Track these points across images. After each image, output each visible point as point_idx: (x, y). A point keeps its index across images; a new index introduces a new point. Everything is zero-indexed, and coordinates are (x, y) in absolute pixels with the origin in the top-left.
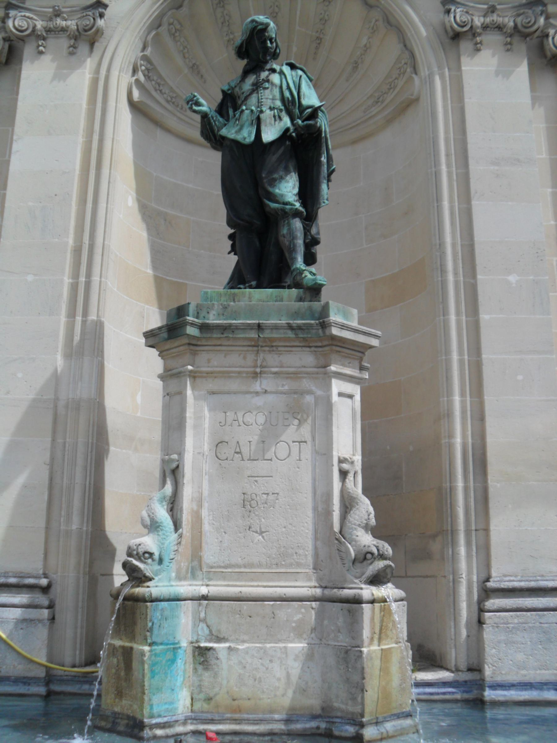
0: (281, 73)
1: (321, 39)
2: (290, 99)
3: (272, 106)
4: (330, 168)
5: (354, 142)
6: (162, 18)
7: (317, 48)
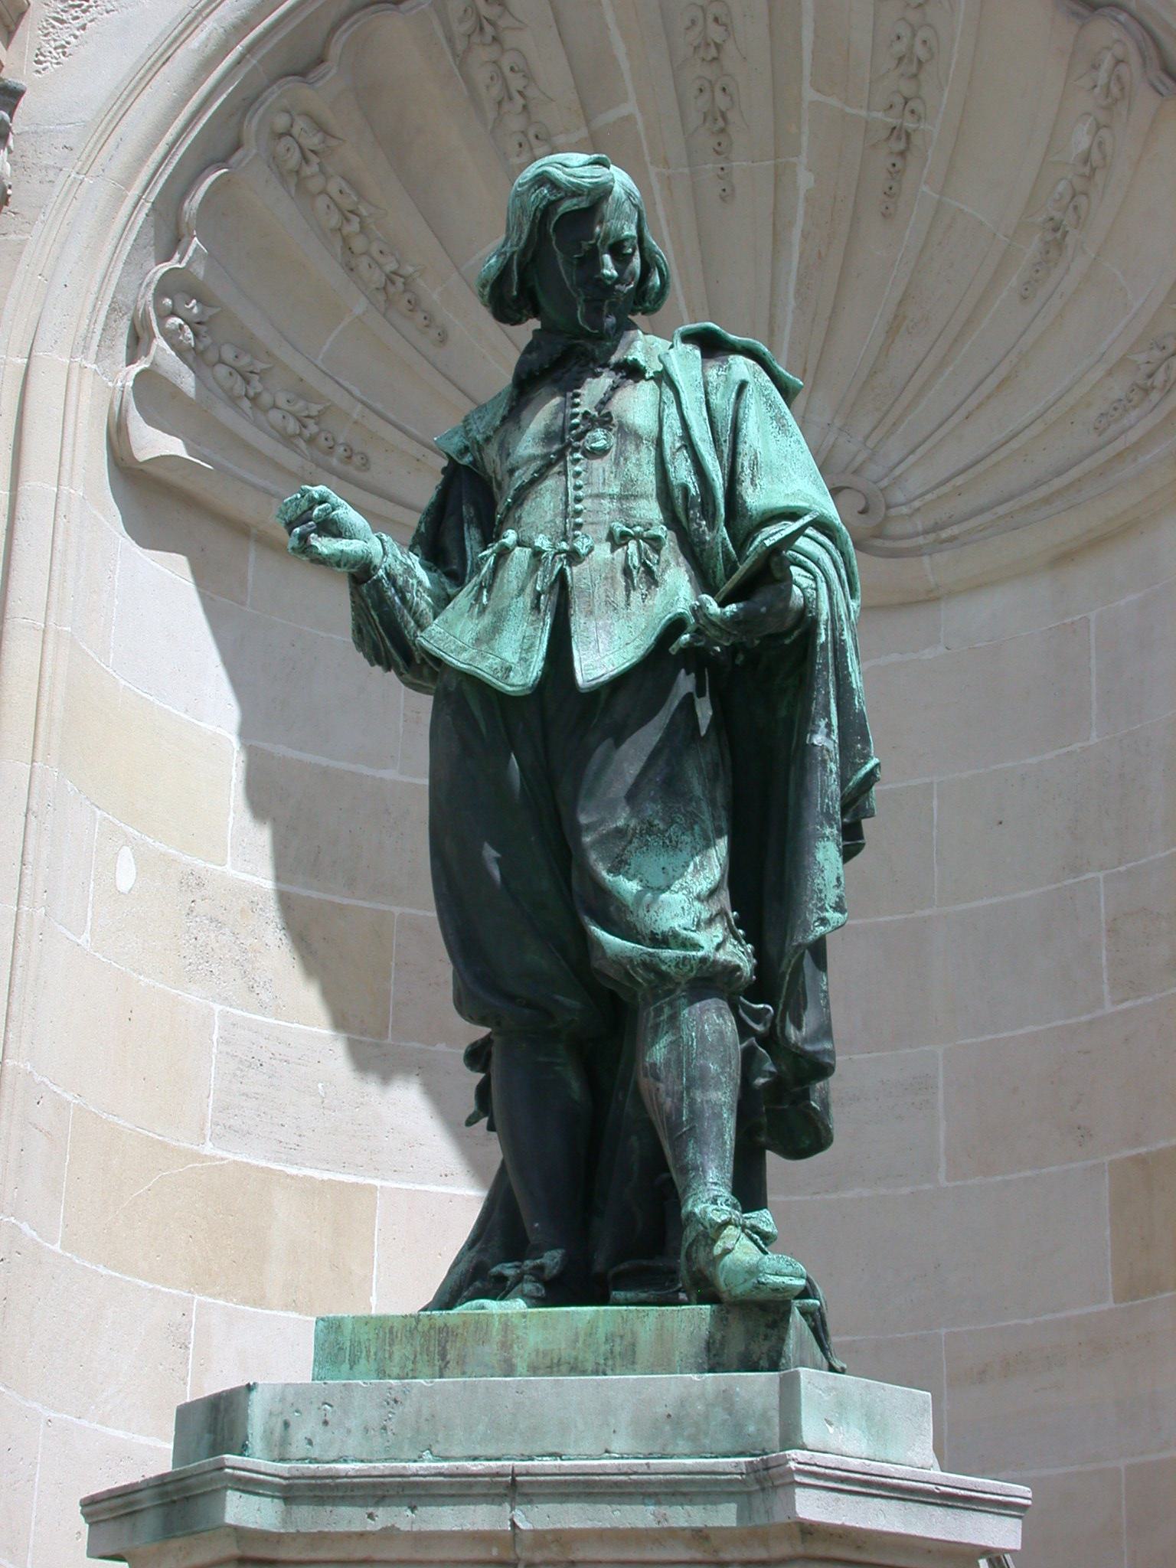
0: (664, 378)
1: (908, 136)
2: (694, 490)
3: (619, 527)
4: (857, 768)
5: (1064, 558)
6: (241, 123)
7: (895, 172)
